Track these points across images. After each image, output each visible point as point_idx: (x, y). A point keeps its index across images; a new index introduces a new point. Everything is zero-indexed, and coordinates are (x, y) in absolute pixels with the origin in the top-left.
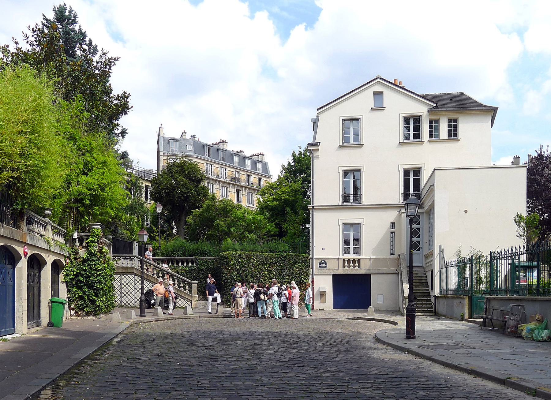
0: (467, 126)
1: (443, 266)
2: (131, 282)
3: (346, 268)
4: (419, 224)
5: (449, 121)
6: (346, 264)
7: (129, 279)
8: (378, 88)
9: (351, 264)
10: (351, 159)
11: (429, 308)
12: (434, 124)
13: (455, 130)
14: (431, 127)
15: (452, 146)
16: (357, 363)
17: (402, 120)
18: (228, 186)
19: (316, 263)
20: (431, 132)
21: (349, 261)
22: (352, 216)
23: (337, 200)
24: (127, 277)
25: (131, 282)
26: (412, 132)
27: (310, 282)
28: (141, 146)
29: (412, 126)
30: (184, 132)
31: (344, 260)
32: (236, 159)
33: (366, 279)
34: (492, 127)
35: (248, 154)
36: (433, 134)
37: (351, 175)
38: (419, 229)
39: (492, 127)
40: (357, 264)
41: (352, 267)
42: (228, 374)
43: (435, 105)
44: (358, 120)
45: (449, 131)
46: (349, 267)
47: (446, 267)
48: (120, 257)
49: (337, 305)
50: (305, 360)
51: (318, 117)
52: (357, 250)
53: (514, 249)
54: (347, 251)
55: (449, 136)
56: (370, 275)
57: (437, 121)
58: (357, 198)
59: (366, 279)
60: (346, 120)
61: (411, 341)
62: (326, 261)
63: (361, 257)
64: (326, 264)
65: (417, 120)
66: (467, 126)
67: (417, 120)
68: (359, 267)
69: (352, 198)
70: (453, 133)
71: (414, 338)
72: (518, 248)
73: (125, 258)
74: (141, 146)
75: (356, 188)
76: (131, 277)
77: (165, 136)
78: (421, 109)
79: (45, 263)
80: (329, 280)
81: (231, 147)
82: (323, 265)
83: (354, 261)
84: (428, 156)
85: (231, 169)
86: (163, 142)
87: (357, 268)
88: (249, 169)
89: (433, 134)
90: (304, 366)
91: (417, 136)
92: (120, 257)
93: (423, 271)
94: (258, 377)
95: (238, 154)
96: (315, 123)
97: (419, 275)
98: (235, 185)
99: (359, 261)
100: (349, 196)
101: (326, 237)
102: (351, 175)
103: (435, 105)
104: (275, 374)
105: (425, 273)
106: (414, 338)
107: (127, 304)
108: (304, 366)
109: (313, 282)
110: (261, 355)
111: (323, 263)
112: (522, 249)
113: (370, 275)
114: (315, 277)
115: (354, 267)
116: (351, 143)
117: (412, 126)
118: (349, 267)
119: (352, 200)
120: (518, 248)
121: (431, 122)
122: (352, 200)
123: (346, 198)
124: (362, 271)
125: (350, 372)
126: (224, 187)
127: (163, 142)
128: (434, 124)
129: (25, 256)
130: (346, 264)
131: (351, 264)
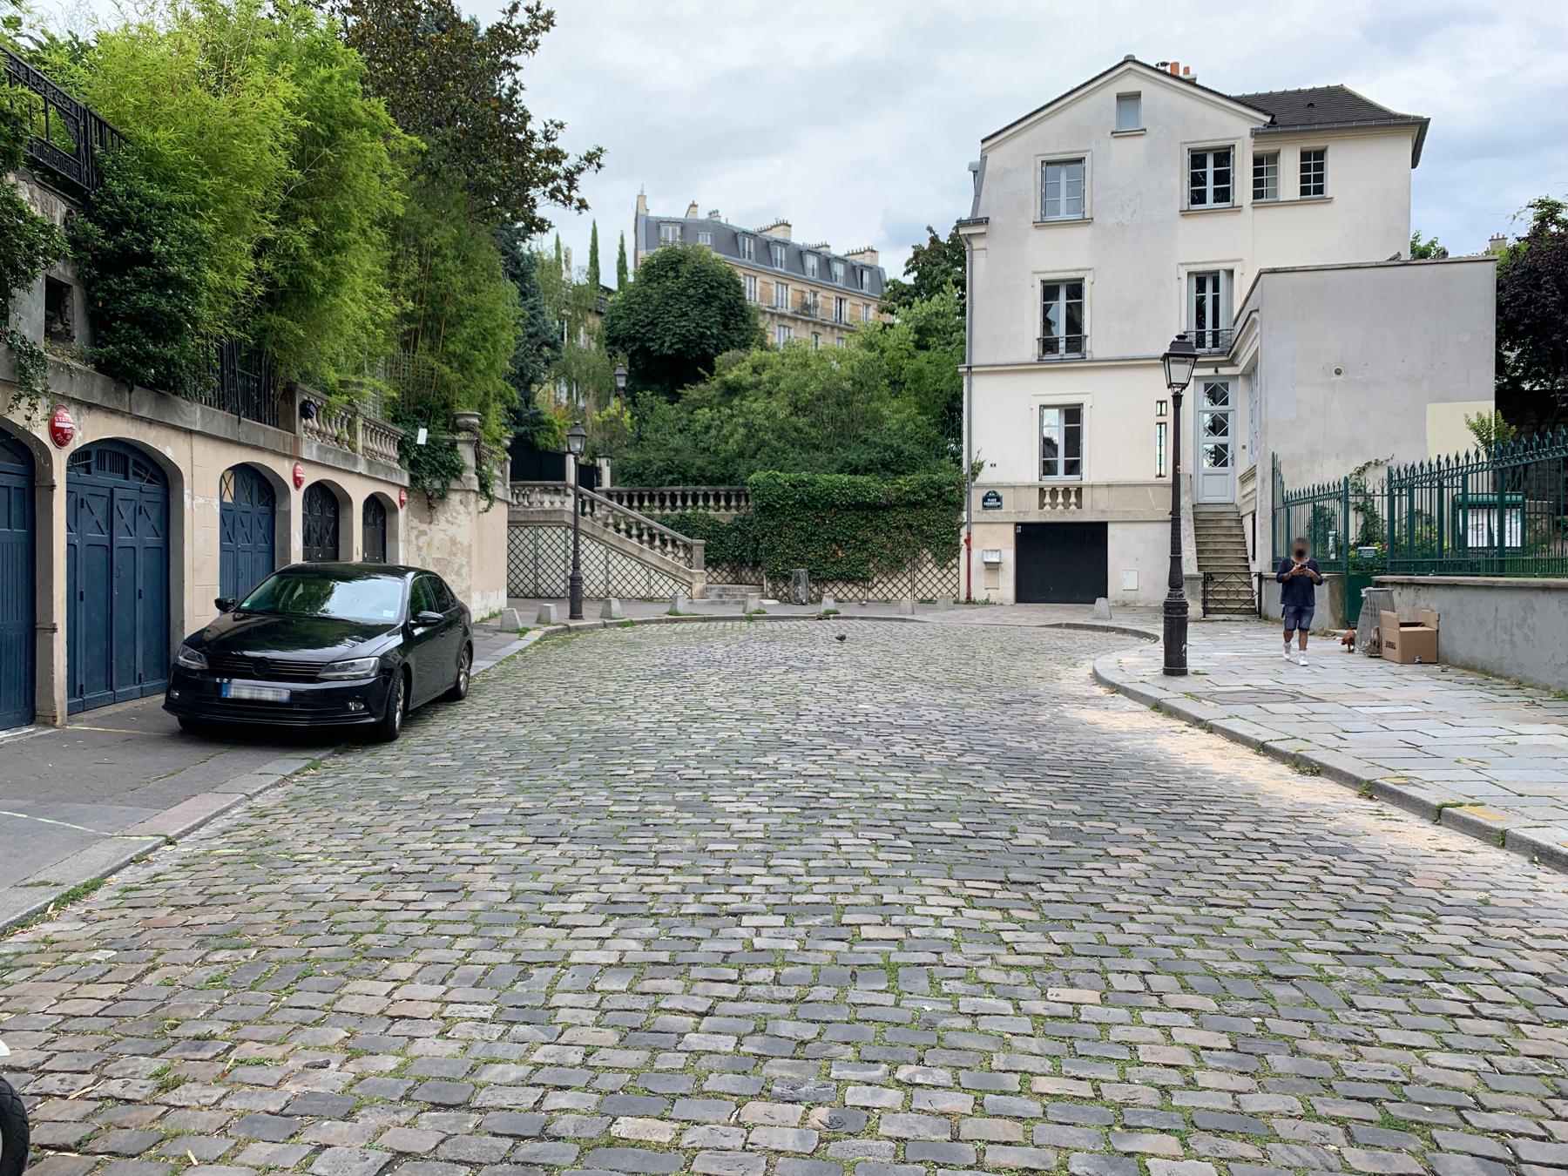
0: (1347, 163)
1: (1279, 504)
3: (1047, 508)
4: (1225, 402)
5: (1305, 156)
6: (1048, 500)
8: (1129, 84)
9: (1060, 499)
10: (1062, 254)
11: (1246, 602)
12: (1263, 165)
13: (1320, 178)
14: (1257, 172)
15: (1312, 213)
16: (1021, 731)
17: (1187, 157)
18: (791, 324)
19: (976, 497)
20: (1257, 183)
21: (1054, 492)
23: (1029, 348)
24: (550, 531)
26: (1210, 187)
27: (962, 541)
28: (588, 237)
29: (1210, 169)
30: (693, 205)
31: (1042, 490)
32: (811, 262)
34: (1414, 165)
35: (838, 250)
36: (1261, 189)
37: (1064, 294)
38: (1226, 416)
39: (1414, 165)
40: (1073, 499)
42: (707, 751)
43: (1268, 119)
44: (1080, 161)
45: (1304, 179)
46: (1054, 506)
47: (1287, 503)
50: (901, 722)
51: (984, 159)
52: (1073, 468)
53: (1443, 460)
54: (1048, 468)
55: (1304, 191)
56: (1104, 525)
57: (1274, 157)
58: (1076, 342)
59: (1093, 536)
60: (1049, 163)
61: (1179, 683)
62: (1000, 493)
63: (1084, 482)
64: (999, 499)
65: (1223, 156)
66: (1347, 163)
67: (1223, 156)
68: (1079, 505)
69: (1062, 344)
70: (1313, 184)
71: (1184, 673)
72: (1452, 458)
73: (545, 490)
74: (588, 237)
75: (1074, 325)
76: (559, 531)
77: (651, 214)
78: (1238, 131)
79: (349, 501)
80: (1009, 534)
81: (799, 237)
82: (992, 502)
83: (1067, 492)
84: (1252, 240)
85: (799, 287)
86: (650, 227)
87: (1073, 507)
89: (1261, 189)
91: (1223, 195)
93: (1234, 516)
94: (769, 760)
95: (814, 252)
96: (978, 172)
97: (1225, 524)
99: (1079, 491)
100: (1057, 341)
101: (1003, 434)
102: (1064, 294)
103: (1268, 119)
105: (1240, 521)
106: (1184, 673)
107: (549, 591)
109: (968, 541)
111: (993, 499)
112: (1473, 460)
113: (1104, 525)
114: (976, 530)
115: (1066, 505)
116: (1063, 216)
117: (1210, 169)
118: (1054, 506)
119: (1062, 351)
120: (1452, 458)
121: (1257, 160)
122: (1062, 351)
123: (1048, 345)
125: (995, 751)
127: (650, 227)
128: (1263, 165)
129: (297, 486)
130: (1048, 500)
131: (1060, 499)
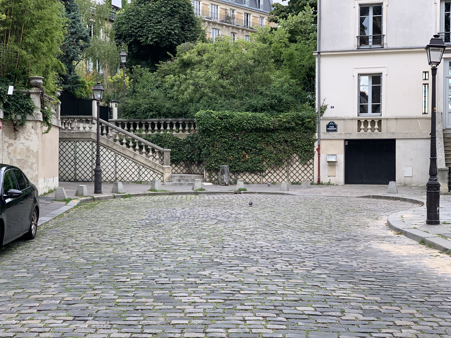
2: (88, 150)
3: (362, 131)
6: (362, 127)
7: (86, 147)
18: (220, 28)
19: (323, 125)
21: (366, 122)
22: (372, 63)
23: (352, 42)
24: (83, 144)
25: (88, 150)
31: (359, 121)
33: (389, 146)
40: (376, 126)
41: (369, 131)
42: (171, 268)
48: (74, 118)
49: (350, 179)
50: (281, 251)
52: (376, 109)
54: (363, 109)
59: (389, 146)
61: (435, 229)
62: (336, 122)
64: (335, 126)
68: (380, 130)
69: (371, 40)
71: (438, 223)
73: (81, 121)
75: (377, 29)
76: (88, 144)
80: (341, 146)
82: (332, 128)
83: (373, 122)
85: (224, 7)
88: (248, 6)
90: (275, 258)
92: (68, 118)
94: (207, 273)
98: (229, 27)
99: (380, 122)
100: (367, 38)
104: (232, 268)
106: (438, 223)
107: (83, 178)
108: (275, 258)
109: (318, 150)
110: (226, 243)
111: (332, 127)
114: (323, 143)
119: (371, 44)
122: (371, 44)
123: (363, 40)
124: (384, 135)
125: (333, 267)
126: (216, 29)
130: (362, 127)
131: (369, 127)
